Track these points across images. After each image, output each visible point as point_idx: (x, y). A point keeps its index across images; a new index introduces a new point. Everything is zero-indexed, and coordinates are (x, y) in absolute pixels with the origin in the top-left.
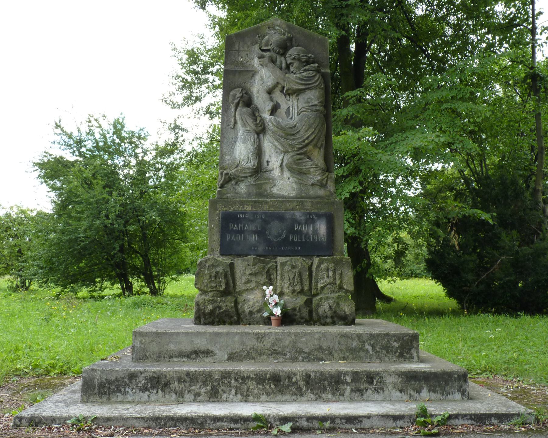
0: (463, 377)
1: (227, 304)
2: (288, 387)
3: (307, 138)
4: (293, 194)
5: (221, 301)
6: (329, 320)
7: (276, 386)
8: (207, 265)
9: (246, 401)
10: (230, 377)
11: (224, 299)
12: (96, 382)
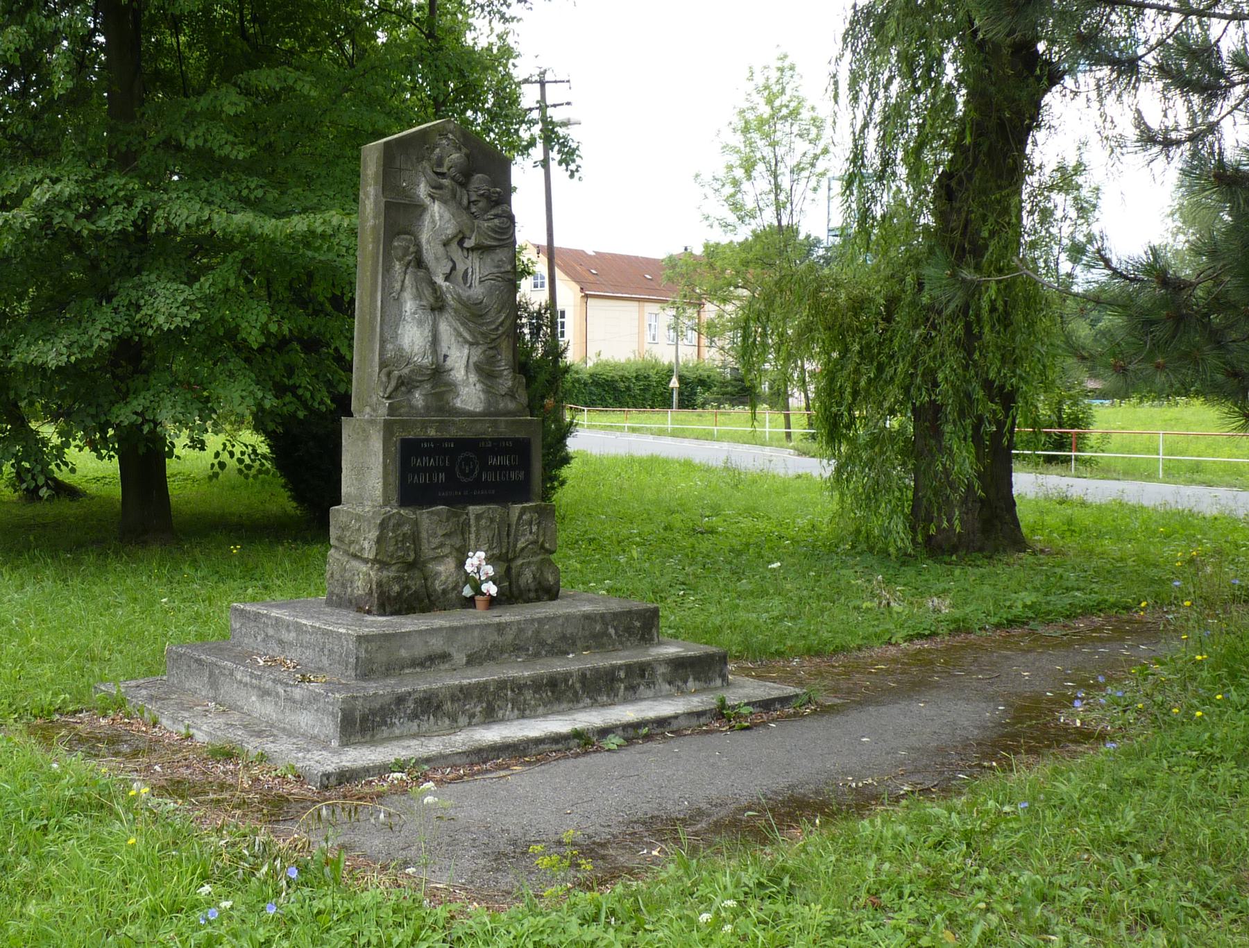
0: (723, 659)
1: (415, 584)
2: (564, 692)
3: (501, 324)
4: (479, 408)
5: (409, 577)
6: (532, 595)
7: (553, 692)
8: (391, 524)
9: (523, 717)
10: (505, 688)
11: (411, 573)
12: (358, 714)
